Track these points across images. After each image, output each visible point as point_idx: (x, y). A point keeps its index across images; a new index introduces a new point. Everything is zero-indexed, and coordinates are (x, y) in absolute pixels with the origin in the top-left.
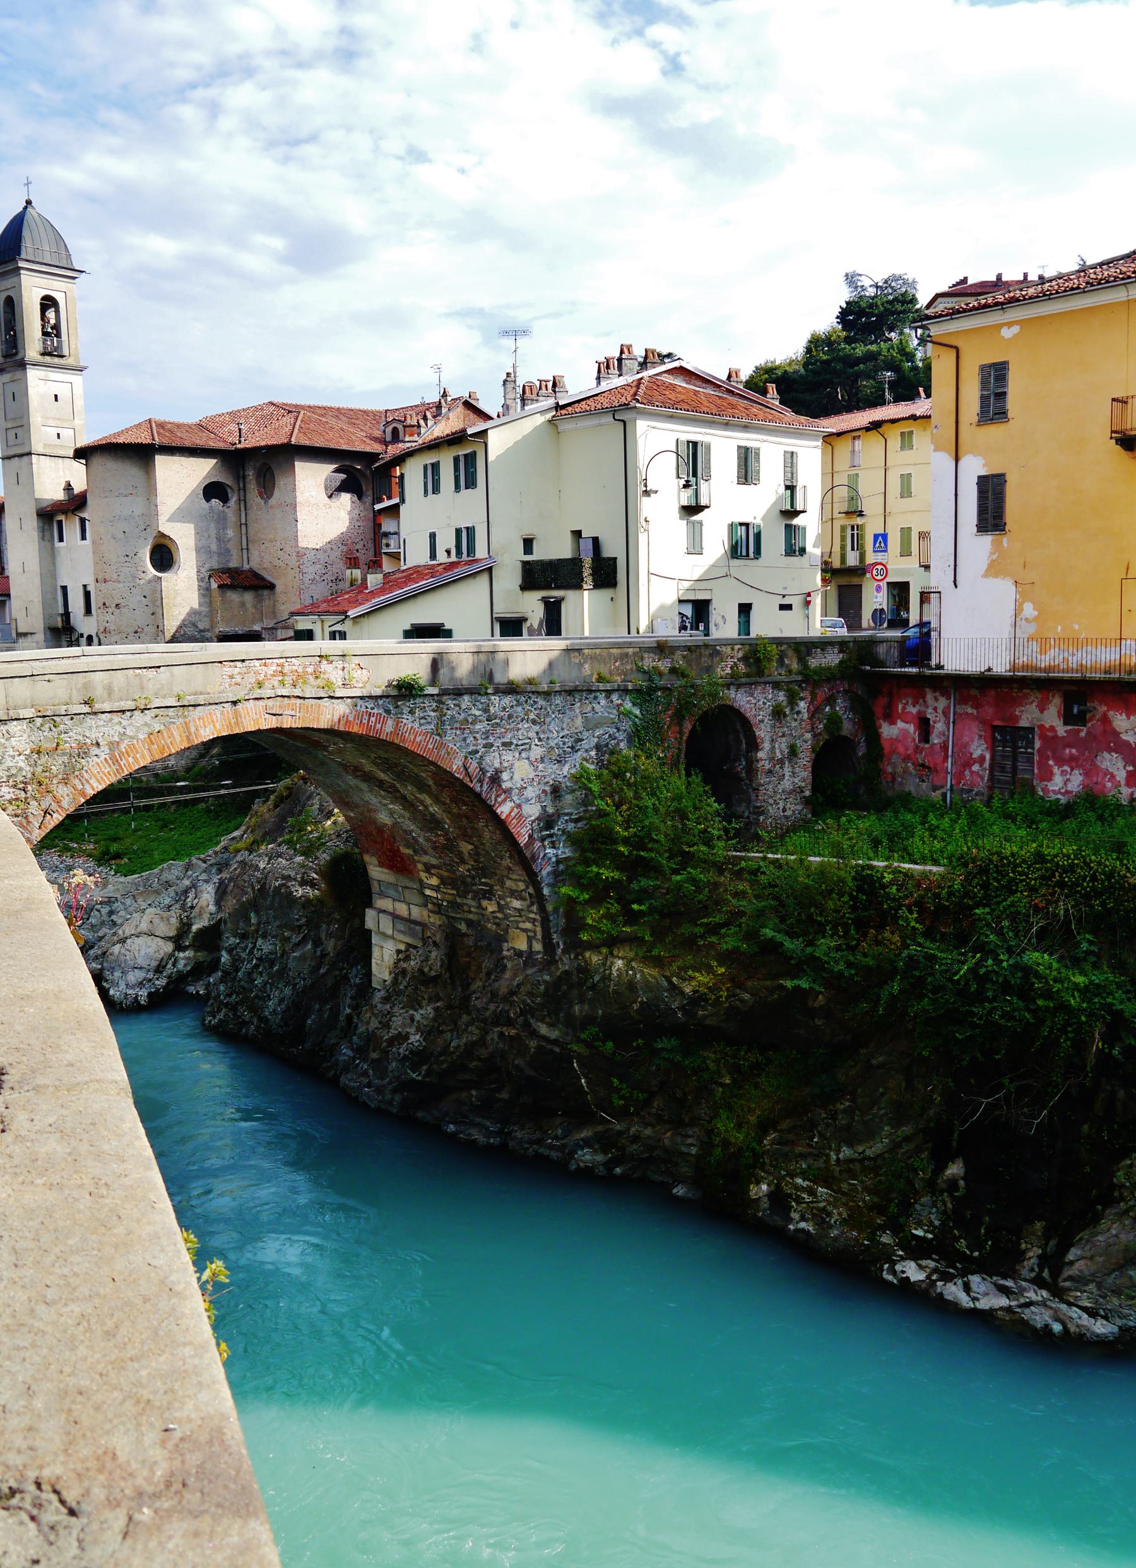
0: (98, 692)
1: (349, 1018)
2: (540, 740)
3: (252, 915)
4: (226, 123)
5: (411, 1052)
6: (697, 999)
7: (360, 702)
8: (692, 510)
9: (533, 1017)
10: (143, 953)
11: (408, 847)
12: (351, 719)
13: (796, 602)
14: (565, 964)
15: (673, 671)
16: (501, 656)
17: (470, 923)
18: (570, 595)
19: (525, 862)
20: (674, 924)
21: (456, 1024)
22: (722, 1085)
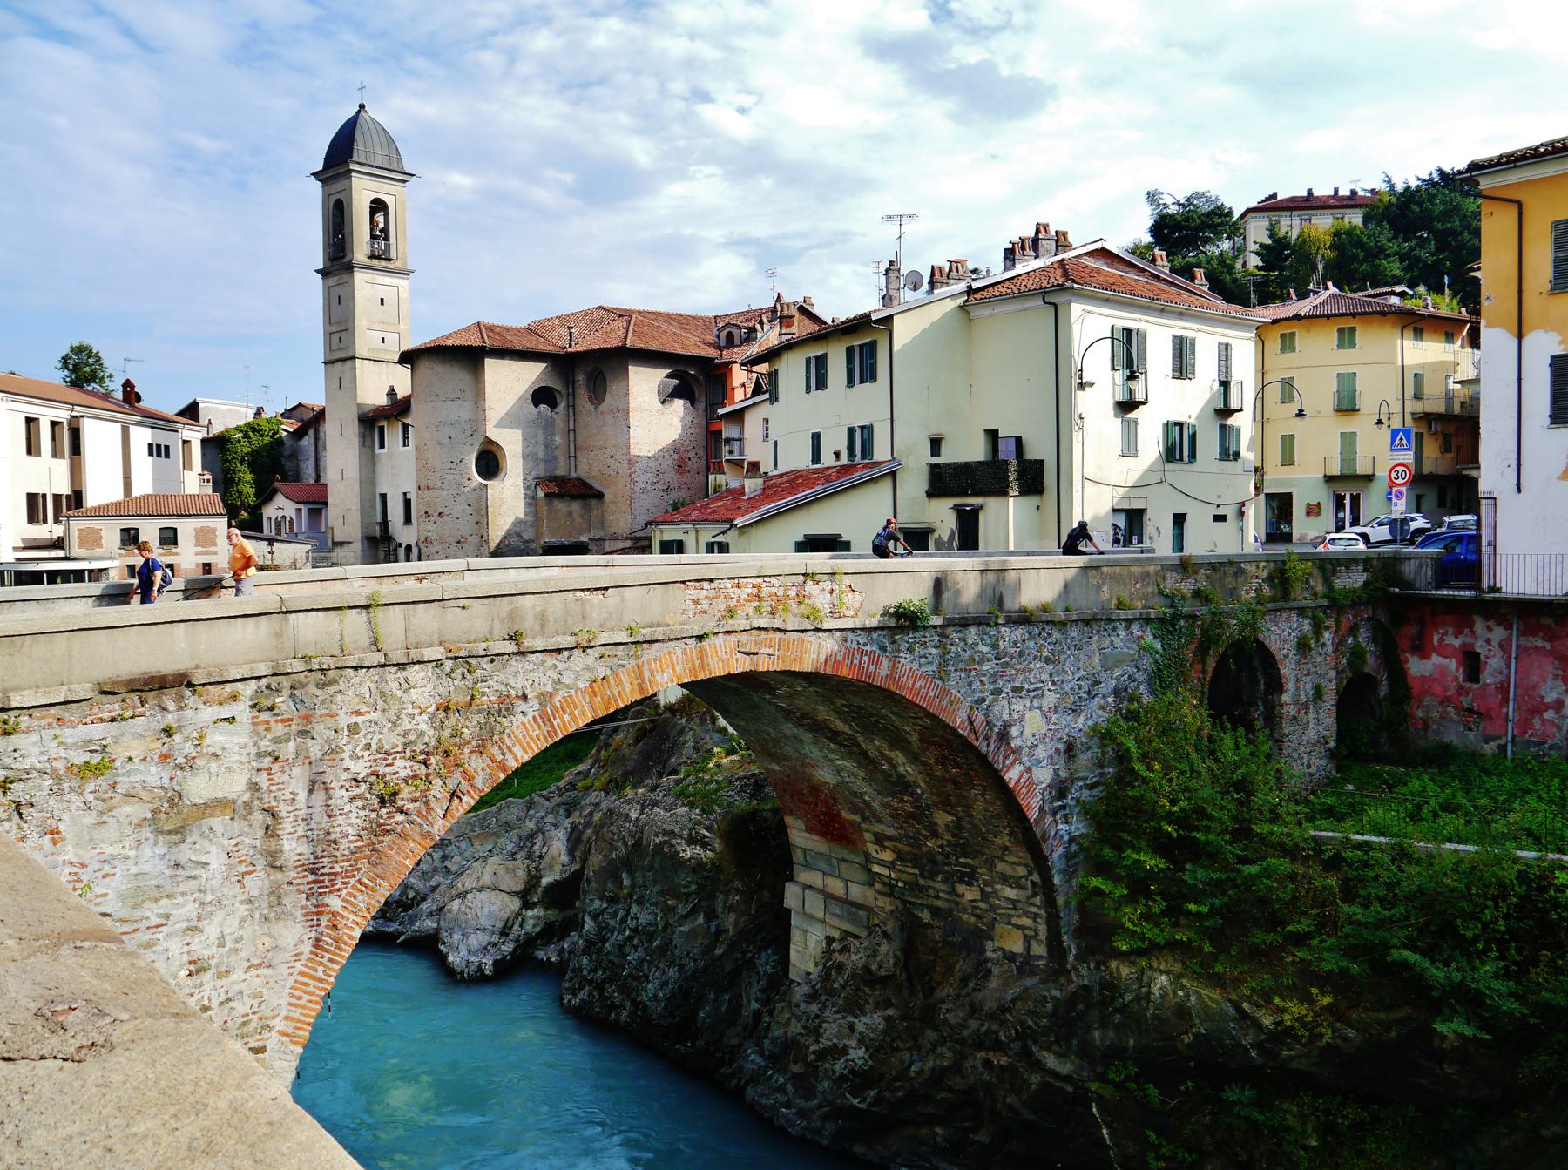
0: (528, 624)
1: (757, 1015)
2: (1054, 683)
3: (624, 875)
4: (523, 68)
5: (852, 1071)
6: (1282, 1035)
7: (850, 636)
8: (1127, 406)
9: (1036, 1042)
10: (486, 910)
11: (854, 811)
12: (840, 658)
13: (1230, 512)
14: (1084, 975)
15: (1197, 594)
16: (1011, 576)
17: (935, 912)
18: (991, 504)
19: (1031, 842)
20: (1242, 928)
21: (916, 1041)
22: (1305, 1148)
